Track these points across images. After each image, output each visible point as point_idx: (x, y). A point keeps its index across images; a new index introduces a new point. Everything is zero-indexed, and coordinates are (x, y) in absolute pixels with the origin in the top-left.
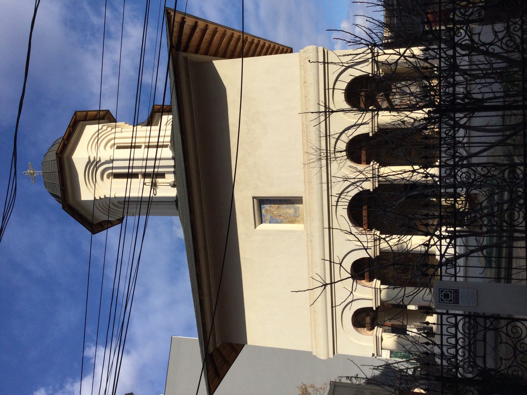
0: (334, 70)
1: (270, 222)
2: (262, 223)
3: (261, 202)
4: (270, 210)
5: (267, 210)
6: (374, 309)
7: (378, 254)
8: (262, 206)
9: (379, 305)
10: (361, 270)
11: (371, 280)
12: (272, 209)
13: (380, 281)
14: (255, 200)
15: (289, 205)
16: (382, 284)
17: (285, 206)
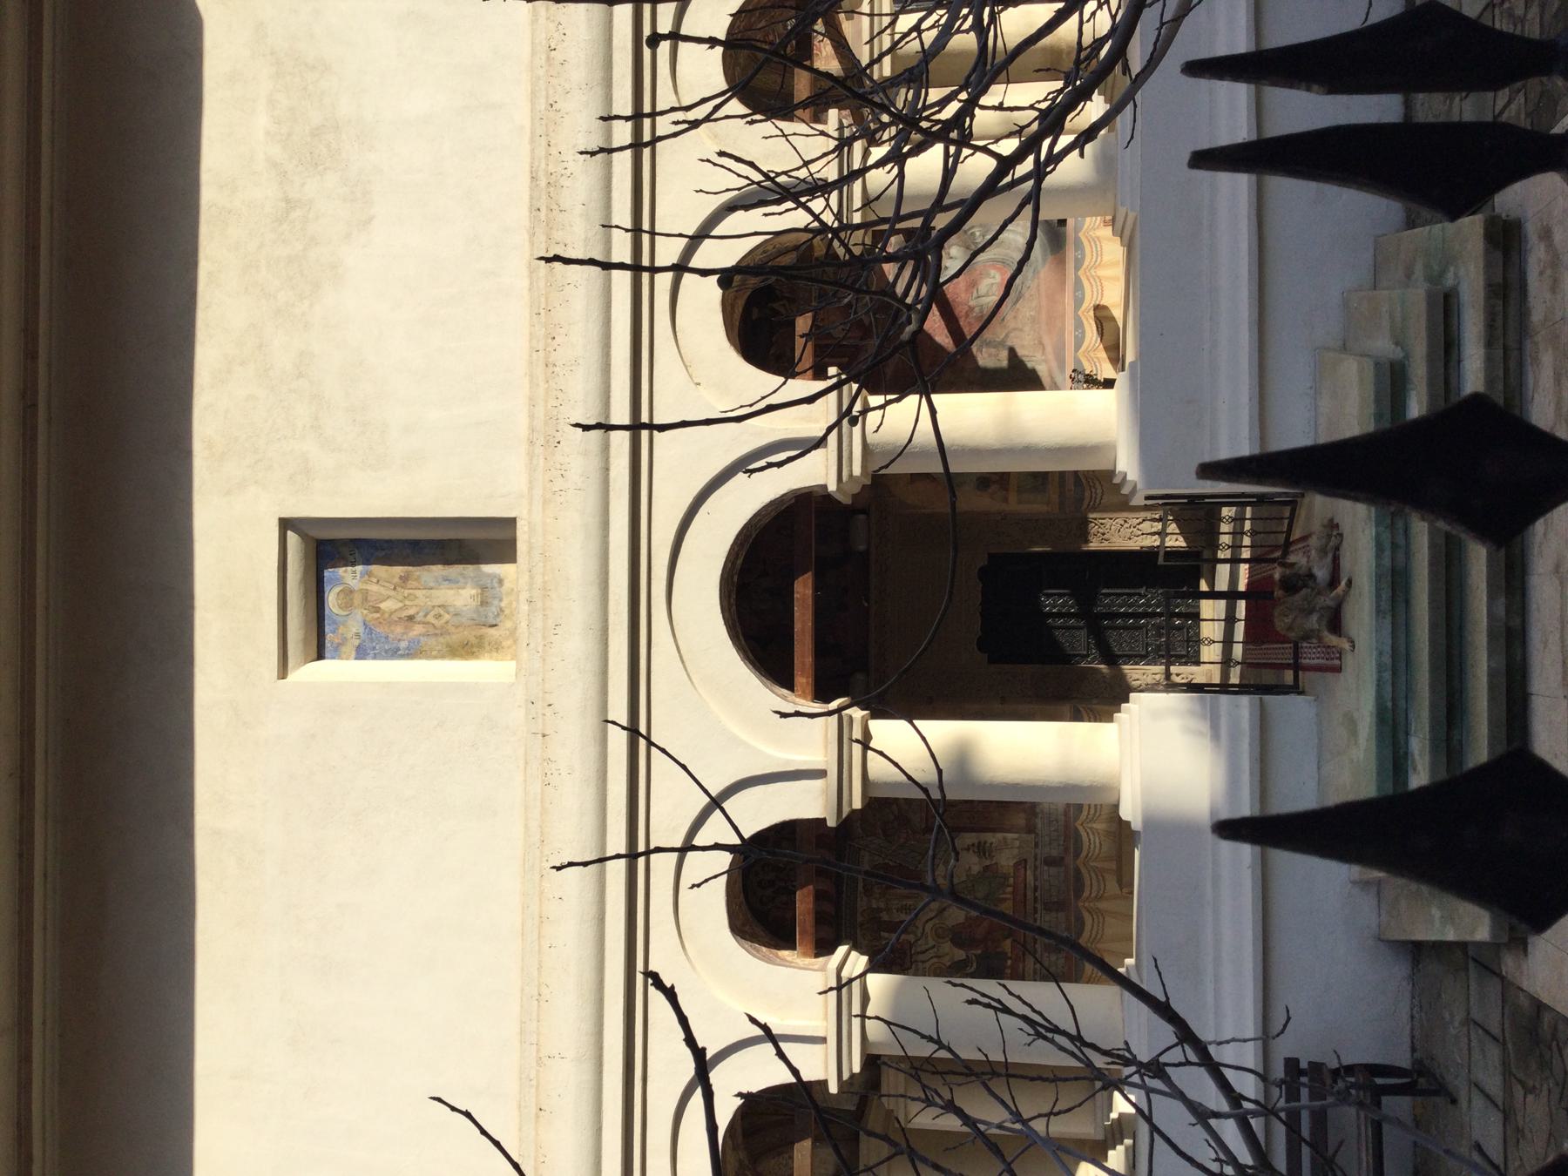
0: (679, 464)
1: (361, 654)
2: (320, 656)
4: (365, 593)
5: (349, 592)
6: (833, 1088)
7: (857, 804)
8: (327, 573)
9: (857, 1069)
10: (784, 886)
11: (824, 948)
12: (374, 588)
13: (865, 959)
14: (292, 537)
15: (455, 570)
16: (873, 967)
17: (438, 570)
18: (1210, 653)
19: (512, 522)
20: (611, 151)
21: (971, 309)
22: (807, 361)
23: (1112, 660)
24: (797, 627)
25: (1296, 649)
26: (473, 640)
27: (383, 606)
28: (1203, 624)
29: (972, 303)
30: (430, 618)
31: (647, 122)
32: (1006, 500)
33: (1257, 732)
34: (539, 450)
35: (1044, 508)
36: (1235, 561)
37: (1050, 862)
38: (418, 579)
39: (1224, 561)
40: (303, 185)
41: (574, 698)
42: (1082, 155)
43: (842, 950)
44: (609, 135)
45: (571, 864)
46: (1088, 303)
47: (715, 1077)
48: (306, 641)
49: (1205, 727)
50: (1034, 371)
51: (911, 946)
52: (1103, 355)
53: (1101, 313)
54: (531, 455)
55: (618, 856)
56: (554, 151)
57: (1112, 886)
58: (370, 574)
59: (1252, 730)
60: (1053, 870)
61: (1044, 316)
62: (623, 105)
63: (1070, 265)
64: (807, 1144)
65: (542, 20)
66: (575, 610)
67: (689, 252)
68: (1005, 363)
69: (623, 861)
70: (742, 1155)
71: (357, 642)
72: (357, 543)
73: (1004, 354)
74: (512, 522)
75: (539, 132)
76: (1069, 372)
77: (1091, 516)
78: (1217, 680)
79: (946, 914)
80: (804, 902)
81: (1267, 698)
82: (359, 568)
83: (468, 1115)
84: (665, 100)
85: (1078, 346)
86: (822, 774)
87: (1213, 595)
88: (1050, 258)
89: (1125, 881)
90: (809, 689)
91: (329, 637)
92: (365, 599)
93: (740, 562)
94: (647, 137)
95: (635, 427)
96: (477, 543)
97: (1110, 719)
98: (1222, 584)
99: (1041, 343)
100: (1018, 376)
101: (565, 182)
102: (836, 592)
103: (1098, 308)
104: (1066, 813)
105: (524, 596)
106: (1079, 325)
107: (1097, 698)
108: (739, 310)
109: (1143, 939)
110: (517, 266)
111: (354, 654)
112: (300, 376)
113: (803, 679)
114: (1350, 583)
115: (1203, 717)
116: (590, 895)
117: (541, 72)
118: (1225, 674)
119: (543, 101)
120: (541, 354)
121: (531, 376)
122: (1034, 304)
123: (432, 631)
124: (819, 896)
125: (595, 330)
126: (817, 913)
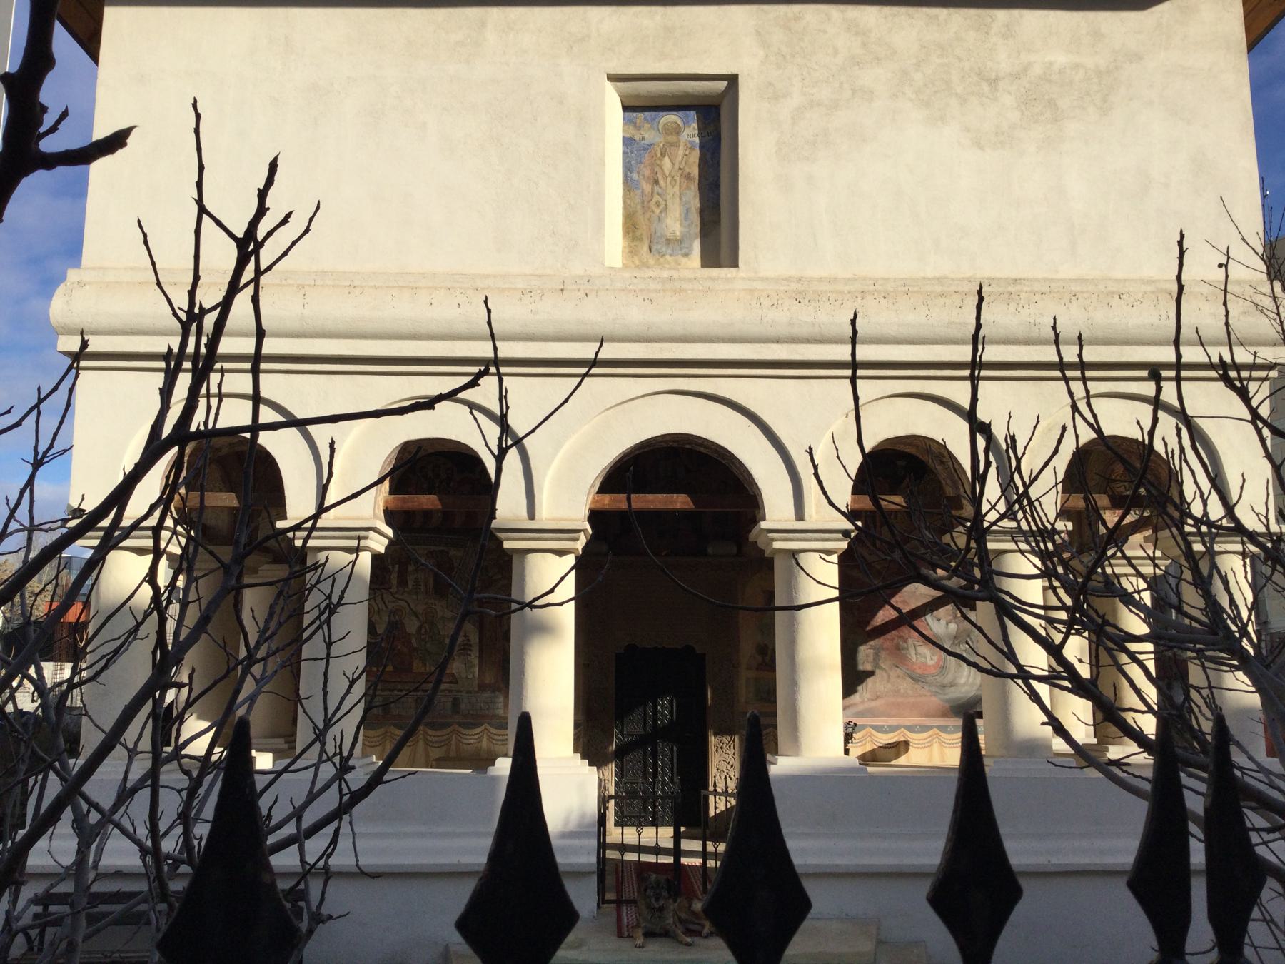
1: (627, 142)
2: (626, 108)
3: (712, 113)
4: (677, 145)
5: (677, 131)
6: (280, 524)
7: (507, 545)
8: (693, 114)
11: (391, 516)
12: (681, 152)
13: (382, 550)
14: (722, 85)
15: (696, 218)
16: (376, 558)
17: (696, 204)
18: (630, 835)
19: (734, 263)
20: (1057, 342)
21: (905, 641)
22: (1071, 504)
23: (619, 755)
24: (650, 497)
25: (634, 902)
26: (638, 233)
27: (667, 159)
28: (653, 830)
29: (910, 641)
30: (656, 198)
31: (1078, 374)
32: (749, 668)
33: (575, 869)
34: (793, 286)
35: (743, 700)
36: (704, 855)
37: (456, 703)
38: (688, 188)
39: (704, 846)
40: (1010, 93)
41: (594, 314)
42: (1043, 724)
43: (389, 532)
44: (1067, 343)
45: (489, 312)
46: (910, 736)
47: (293, 432)
48: (638, 96)
49: (572, 827)
50: (855, 691)
51: (387, 589)
52: (868, 748)
53: (902, 748)
54: (788, 279)
55: (495, 349)
56: (1037, 297)
57: (436, 753)
58: (692, 148)
59: (570, 865)
60: (449, 705)
61: (900, 700)
62: (1090, 355)
63: (941, 722)
64: (235, 503)
65: (1144, 288)
66: (663, 316)
67: (1169, 409)
68: (861, 668)
69: (492, 355)
70: (225, 451)
71: (637, 138)
72: (717, 138)
73: (868, 667)
74: (734, 263)
75: (1053, 285)
76: (854, 720)
77: (737, 738)
78: (608, 840)
79: (414, 618)
80: (428, 501)
81: (595, 878)
82: (697, 140)
83: (307, 231)
84: (1094, 387)
85: (876, 728)
86: (532, 515)
87: (677, 837)
88: (947, 705)
89: (441, 762)
90: (599, 506)
91: (641, 115)
92: (672, 145)
93: (702, 450)
94: (1069, 374)
95: (854, 365)
96: (718, 234)
97: (575, 751)
98: (686, 845)
99: (878, 697)
100: (852, 679)
101: (1013, 305)
102: (679, 527)
103: (906, 744)
104: (495, 716)
105: (675, 274)
106: (893, 729)
107: (590, 743)
108: (908, 450)
109: (422, 780)
110: (985, 271)
111: (627, 135)
112: (854, 91)
113: (607, 501)
114: (689, 945)
115: (580, 825)
116: (462, 328)
117: (1101, 287)
118: (615, 847)
119: (1079, 289)
120: (872, 288)
121: (855, 280)
122: (910, 692)
123: (646, 199)
124: (427, 514)
125: (892, 331)
126: (414, 511)
